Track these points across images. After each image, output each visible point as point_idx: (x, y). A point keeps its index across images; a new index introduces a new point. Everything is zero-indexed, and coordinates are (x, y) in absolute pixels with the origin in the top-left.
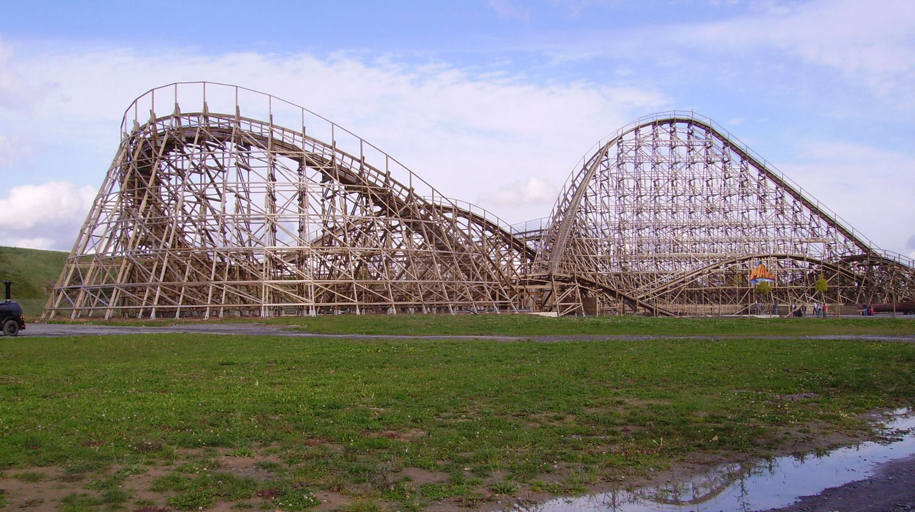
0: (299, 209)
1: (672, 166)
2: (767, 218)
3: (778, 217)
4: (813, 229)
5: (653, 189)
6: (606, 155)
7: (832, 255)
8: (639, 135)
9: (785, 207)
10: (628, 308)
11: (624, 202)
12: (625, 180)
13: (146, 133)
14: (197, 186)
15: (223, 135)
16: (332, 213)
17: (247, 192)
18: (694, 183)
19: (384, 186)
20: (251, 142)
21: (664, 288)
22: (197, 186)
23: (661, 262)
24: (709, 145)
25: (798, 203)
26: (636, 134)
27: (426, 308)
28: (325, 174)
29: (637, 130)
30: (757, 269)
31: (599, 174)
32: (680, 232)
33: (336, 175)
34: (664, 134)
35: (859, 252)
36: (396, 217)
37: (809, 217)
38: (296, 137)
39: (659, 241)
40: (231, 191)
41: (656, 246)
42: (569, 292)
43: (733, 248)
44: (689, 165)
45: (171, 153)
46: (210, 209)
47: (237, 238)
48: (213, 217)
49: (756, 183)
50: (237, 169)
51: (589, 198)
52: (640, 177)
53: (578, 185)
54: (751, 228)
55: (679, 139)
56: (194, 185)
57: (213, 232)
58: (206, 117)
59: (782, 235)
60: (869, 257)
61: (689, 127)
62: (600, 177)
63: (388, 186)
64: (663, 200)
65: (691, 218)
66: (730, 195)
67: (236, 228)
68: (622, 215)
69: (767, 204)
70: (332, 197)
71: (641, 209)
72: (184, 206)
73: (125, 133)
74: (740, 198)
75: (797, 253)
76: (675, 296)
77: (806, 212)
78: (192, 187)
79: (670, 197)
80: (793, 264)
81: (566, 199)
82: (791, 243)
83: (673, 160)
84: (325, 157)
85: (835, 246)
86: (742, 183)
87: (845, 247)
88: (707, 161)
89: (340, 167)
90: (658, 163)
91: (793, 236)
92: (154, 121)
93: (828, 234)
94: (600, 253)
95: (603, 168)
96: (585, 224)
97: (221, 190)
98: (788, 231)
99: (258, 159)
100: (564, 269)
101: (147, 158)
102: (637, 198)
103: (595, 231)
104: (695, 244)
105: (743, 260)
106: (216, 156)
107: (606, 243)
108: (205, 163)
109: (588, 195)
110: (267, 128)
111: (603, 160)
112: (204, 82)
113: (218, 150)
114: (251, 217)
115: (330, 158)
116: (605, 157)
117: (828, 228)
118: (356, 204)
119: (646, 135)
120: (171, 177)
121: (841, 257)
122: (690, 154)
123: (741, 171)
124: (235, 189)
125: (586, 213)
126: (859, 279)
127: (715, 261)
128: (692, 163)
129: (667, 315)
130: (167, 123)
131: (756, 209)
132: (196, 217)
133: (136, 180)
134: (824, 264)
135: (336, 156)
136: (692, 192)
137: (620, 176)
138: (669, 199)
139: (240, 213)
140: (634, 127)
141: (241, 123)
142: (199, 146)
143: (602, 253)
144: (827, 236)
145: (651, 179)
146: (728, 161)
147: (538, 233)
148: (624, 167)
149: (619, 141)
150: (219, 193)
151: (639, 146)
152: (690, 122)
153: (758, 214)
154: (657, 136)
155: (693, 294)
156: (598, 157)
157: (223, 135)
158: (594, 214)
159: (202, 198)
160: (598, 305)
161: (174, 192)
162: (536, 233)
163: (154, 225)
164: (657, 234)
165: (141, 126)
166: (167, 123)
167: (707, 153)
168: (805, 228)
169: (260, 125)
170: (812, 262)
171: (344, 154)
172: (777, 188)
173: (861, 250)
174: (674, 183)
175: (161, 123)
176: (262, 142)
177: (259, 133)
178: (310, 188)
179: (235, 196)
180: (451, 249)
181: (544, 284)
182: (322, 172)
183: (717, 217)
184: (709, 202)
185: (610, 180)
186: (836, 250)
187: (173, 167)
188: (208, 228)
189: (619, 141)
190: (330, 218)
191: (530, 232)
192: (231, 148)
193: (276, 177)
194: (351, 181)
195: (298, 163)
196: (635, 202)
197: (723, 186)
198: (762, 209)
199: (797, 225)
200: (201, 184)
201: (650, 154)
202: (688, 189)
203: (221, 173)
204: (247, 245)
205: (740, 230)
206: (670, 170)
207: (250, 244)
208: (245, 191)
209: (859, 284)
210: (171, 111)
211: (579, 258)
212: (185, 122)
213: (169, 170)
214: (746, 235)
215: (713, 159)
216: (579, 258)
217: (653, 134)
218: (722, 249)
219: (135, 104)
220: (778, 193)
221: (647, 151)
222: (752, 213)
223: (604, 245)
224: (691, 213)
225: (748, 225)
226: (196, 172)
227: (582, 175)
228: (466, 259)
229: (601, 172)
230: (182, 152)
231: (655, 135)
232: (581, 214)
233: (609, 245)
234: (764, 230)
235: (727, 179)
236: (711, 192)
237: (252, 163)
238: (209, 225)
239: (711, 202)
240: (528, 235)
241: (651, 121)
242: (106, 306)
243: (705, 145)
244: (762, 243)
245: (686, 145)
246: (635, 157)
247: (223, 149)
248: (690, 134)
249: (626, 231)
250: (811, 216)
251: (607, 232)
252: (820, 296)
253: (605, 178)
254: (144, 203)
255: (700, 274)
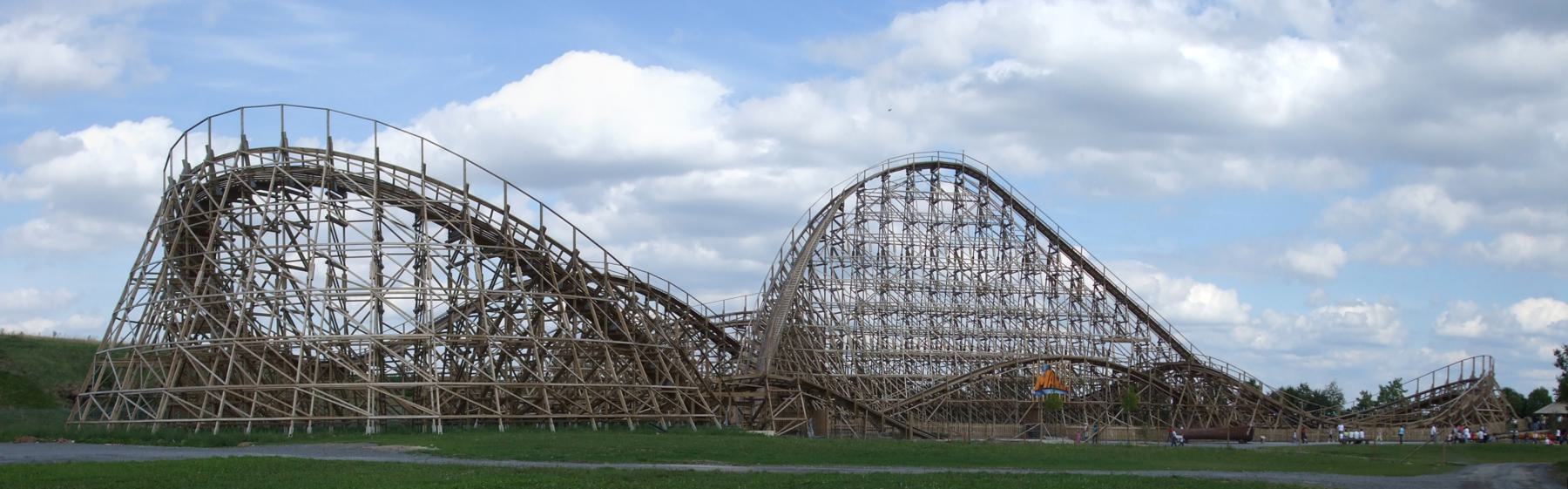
0: (415, 278)
1: (932, 227)
2: (1058, 306)
3: (1073, 305)
4: (1118, 324)
5: (904, 259)
6: (840, 209)
7: (1142, 361)
8: (889, 182)
9: (1083, 292)
10: (868, 425)
11: (864, 275)
12: (866, 245)
13: (201, 178)
14: (271, 249)
15: (308, 178)
16: (463, 286)
17: (343, 257)
18: (962, 253)
19: (537, 247)
20: (348, 187)
21: (917, 399)
22: (271, 249)
23: (912, 362)
24: (984, 202)
25: (1101, 288)
26: (883, 181)
27: (597, 422)
28: (453, 230)
29: (885, 175)
30: (1045, 376)
31: (830, 234)
32: (940, 320)
33: (468, 231)
34: (922, 182)
35: (1176, 358)
36: (554, 291)
37: (1114, 307)
38: (413, 178)
39: (911, 332)
40: (321, 256)
41: (907, 339)
42: (787, 403)
43: (1012, 345)
44: (956, 228)
45: (235, 205)
46: (290, 281)
47: (329, 324)
48: (294, 293)
49: (1046, 258)
50: (329, 225)
51: (816, 268)
52: (887, 241)
53: (799, 249)
54: (1037, 319)
55: (943, 191)
56: (268, 248)
57: (296, 315)
58: (285, 153)
59: (1078, 330)
60: (1189, 364)
61: (957, 176)
62: (832, 239)
63: (542, 248)
64: (919, 276)
65: (956, 301)
66: (1010, 272)
67: (327, 308)
68: (861, 294)
69: (1059, 286)
70: (464, 263)
71: (887, 286)
72: (255, 277)
73: (171, 179)
74: (1023, 276)
75: (1096, 355)
76: (932, 411)
77: (1111, 300)
78: (265, 250)
79: (928, 271)
80: (1092, 370)
81: (783, 268)
82: (1090, 343)
83: (934, 219)
84: (454, 206)
85: (1147, 349)
86: (1027, 255)
87: (1159, 350)
88: (980, 223)
89: (475, 221)
90: (913, 223)
91: (1092, 331)
92: (212, 159)
93: (1137, 331)
94: (828, 346)
95: (836, 227)
96: (808, 306)
97: (306, 255)
98: (1086, 324)
99: (358, 210)
100: (779, 368)
101: (203, 212)
102: (882, 270)
103: (822, 314)
104: (961, 339)
105: (1025, 363)
106: (300, 206)
107: (838, 333)
108: (284, 216)
109: (814, 263)
110: (372, 166)
111: (836, 215)
112: (282, 105)
113: (301, 199)
114: (348, 292)
115: (460, 208)
116: (839, 211)
117: (1138, 323)
118: (497, 274)
119: (898, 182)
120: (234, 237)
121: (1154, 364)
122: (957, 212)
123: (1026, 240)
124: (327, 253)
125: (811, 289)
126: (1176, 395)
127: (986, 363)
128: (959, 225)
129: (923, 437)
130: (230, 162)
131: (1045, 293)
132: (272, 293)
133: (187, 243)
134: (1133, 372)
135: (470, 205)
136: (958, 265)
137: (860, 239)
138: (926, 274)
139: (333, 287)
140: (880, 170)
141: (335, 161)
142: (274, 193)
143: (831, 347)
144: (1137, 335)
145: (902, 245)
146: (1010, 224)
147: (740, 317)
148: (866, 227)
149: (860, 189)
150: (303, 259)
151: (888, 198)
152: (959, 168)
153: (1047, 300)
154: (913, 185)
155: (959, 411)
156: (829, 211)
157: (308, 178)
158: (822, 291)
159: (278, 264)
160: (829, 422)
161: (240, 259)
162: (739, 316)
163: (212, 305)
164: (907, 323)
165: (192, 168)
166: (230, 162)
167: (981, 213)
168: (1108, 323)
169: (360, 163)
170: (1117, 368)
171: (480, 202)
172: (1073, 266)
173: (1178, 356)
174: (935, 251)
175: (221, 162)
176: (363, 185)
177: (359, 174)
178: (434, 250)
179: (327, 263)
180: (630, 337)
181: (753, 389)
182: (449, 227)
183: (990, 301)
184: (982, 281)
185: (845, 244)
186: (1147, 354)
187: (237, 223)
188: (289, 307)
189: (860, 189)
190: (460, 292)
191: (730, 315)
192: (322, 196)
193: (384, 235)
194: (491, 241)
195: (414, 215)
196: (879, 276)
197: (1000, 259)
198: (1052, 293)
199: (1097, 318)
200: (277, 247)
201: (902, 209)
202: (953, 261)
203: (305, 231)
204: (342, 332)
205: (1021, 321)
206: (929, 233)
207: (346, 332)
208: (339, 256)
209: (1176, 401)
210: (234, 145)
211: (801, 354)
212: (255, 161)
213: (231, 228)
214: (1030, 329)
215: (989, 221)
216: (801, 354)
217: (907, 182)
218: (996, 347)
219: (184, 138)
220: (1074, 273)
221: (898, 205)
222: (1039, 298)
223: (835, 336)
224: (955, 294)
225: (1033, 315)
226: (272, 231)
227: (806, 236)
228: (652, 354)
229: (833, 232)
230: (252, 203)
231: (910, 184)
232: (804, 290)
233: (842, 336)
234: (1054, 323)
235: (1006, 249)
236: (985, 267)
237: (350, 215)
238: (290, 304)
239: (984, 280)
240: (727, 319)
241: (904, 163)
242: (151, 418)
243: (979, 201)
244: (1051, 340)
245: (953, 200)
246: (881, 213)
247: (308, 197)
248: (957, 185)
249: (866, 317)
250: (1117, 306)
251: (839, 317)
252: (1126, 415)
253: (838, 241)
254: (200, 274)
255: (968, 381)
